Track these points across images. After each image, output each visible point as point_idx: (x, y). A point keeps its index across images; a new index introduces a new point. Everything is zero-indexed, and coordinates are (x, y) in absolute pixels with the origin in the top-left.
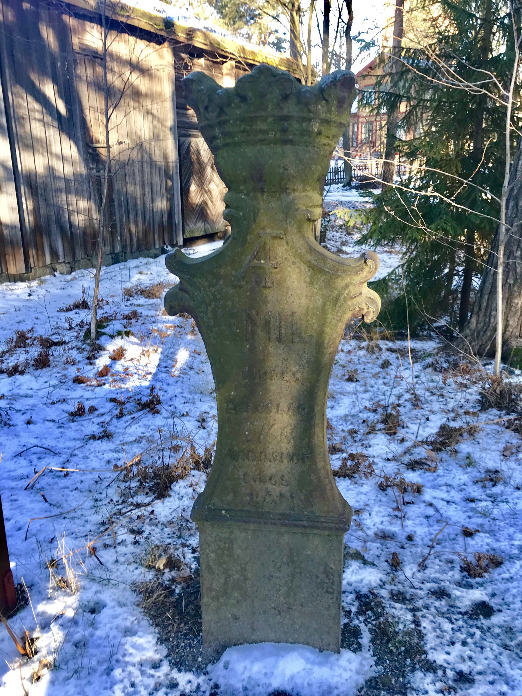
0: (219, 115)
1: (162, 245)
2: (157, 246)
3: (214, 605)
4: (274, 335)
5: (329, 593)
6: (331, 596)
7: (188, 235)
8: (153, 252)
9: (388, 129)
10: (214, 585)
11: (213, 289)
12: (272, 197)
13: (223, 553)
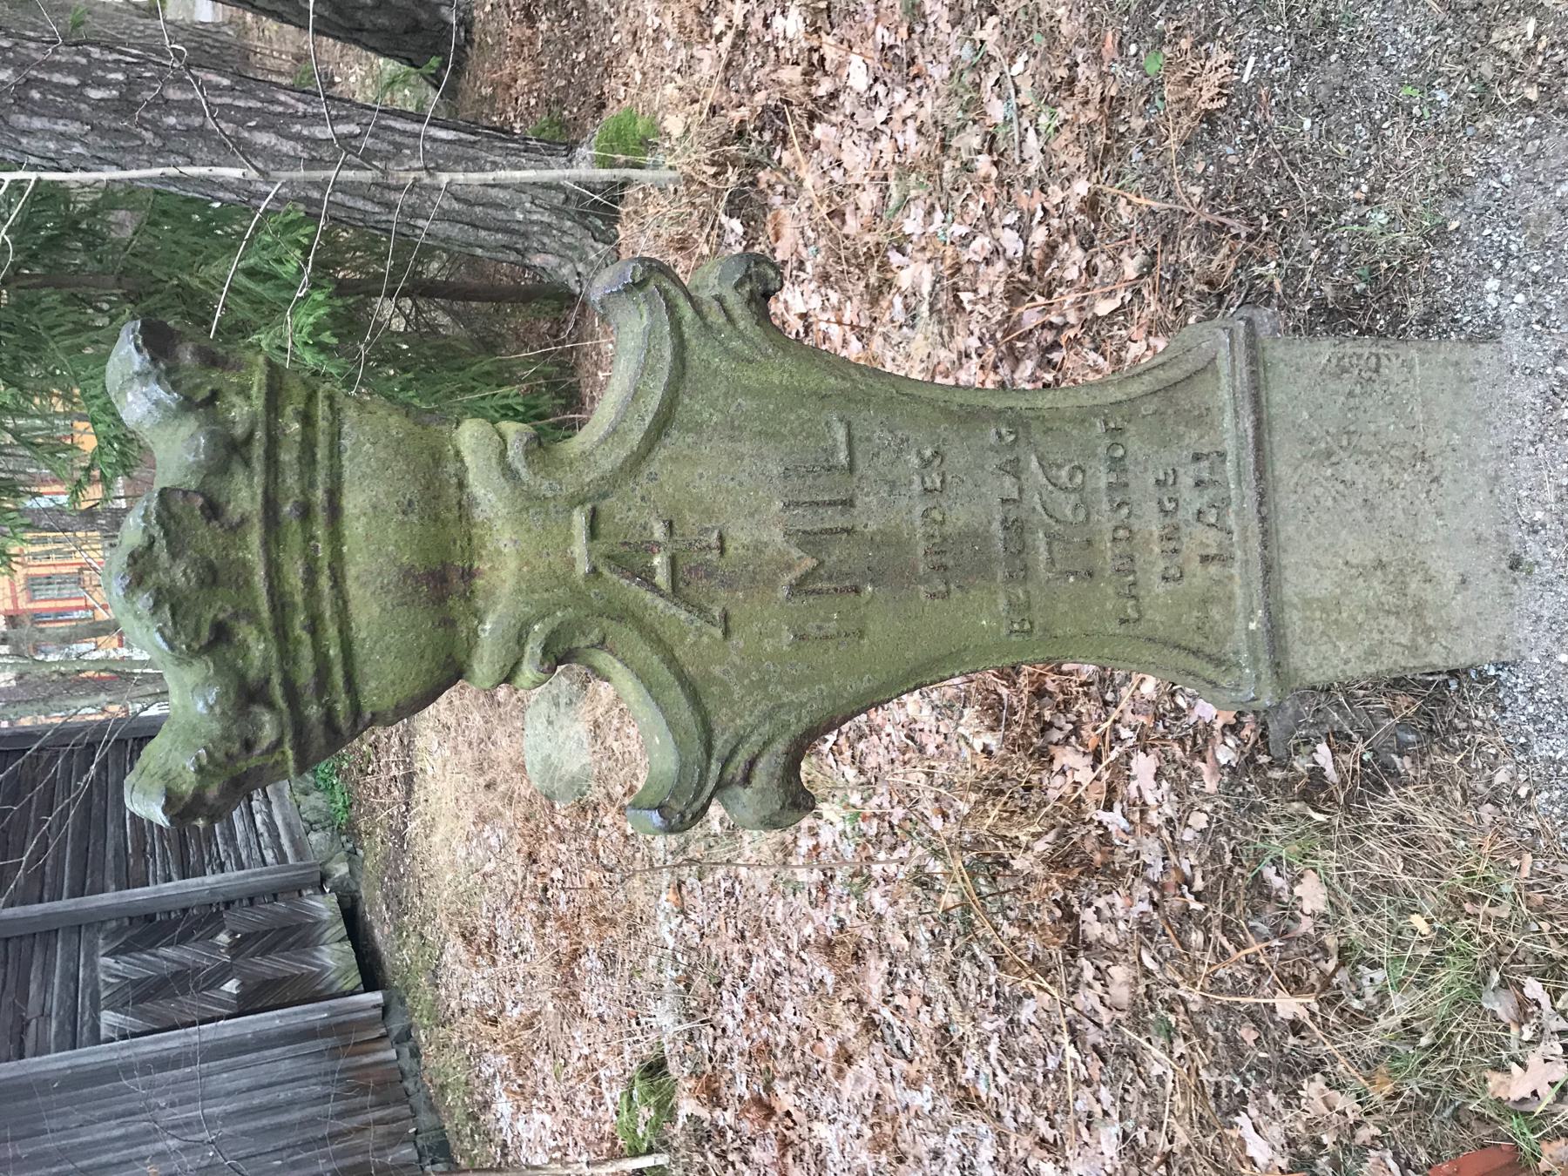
0: (270, 705)
1: (387, 1043)
2: (392, 1054)
3: (1444, 639)
4: (834, 519)
5: (1378, 365)
6: (1384, 361)
7: (355, 979)
8: (407, 1063)
9: (50, 509)
10: (1404, 641)
11: (737, 692)
12: (484, 546)
13: (1336, 622)
